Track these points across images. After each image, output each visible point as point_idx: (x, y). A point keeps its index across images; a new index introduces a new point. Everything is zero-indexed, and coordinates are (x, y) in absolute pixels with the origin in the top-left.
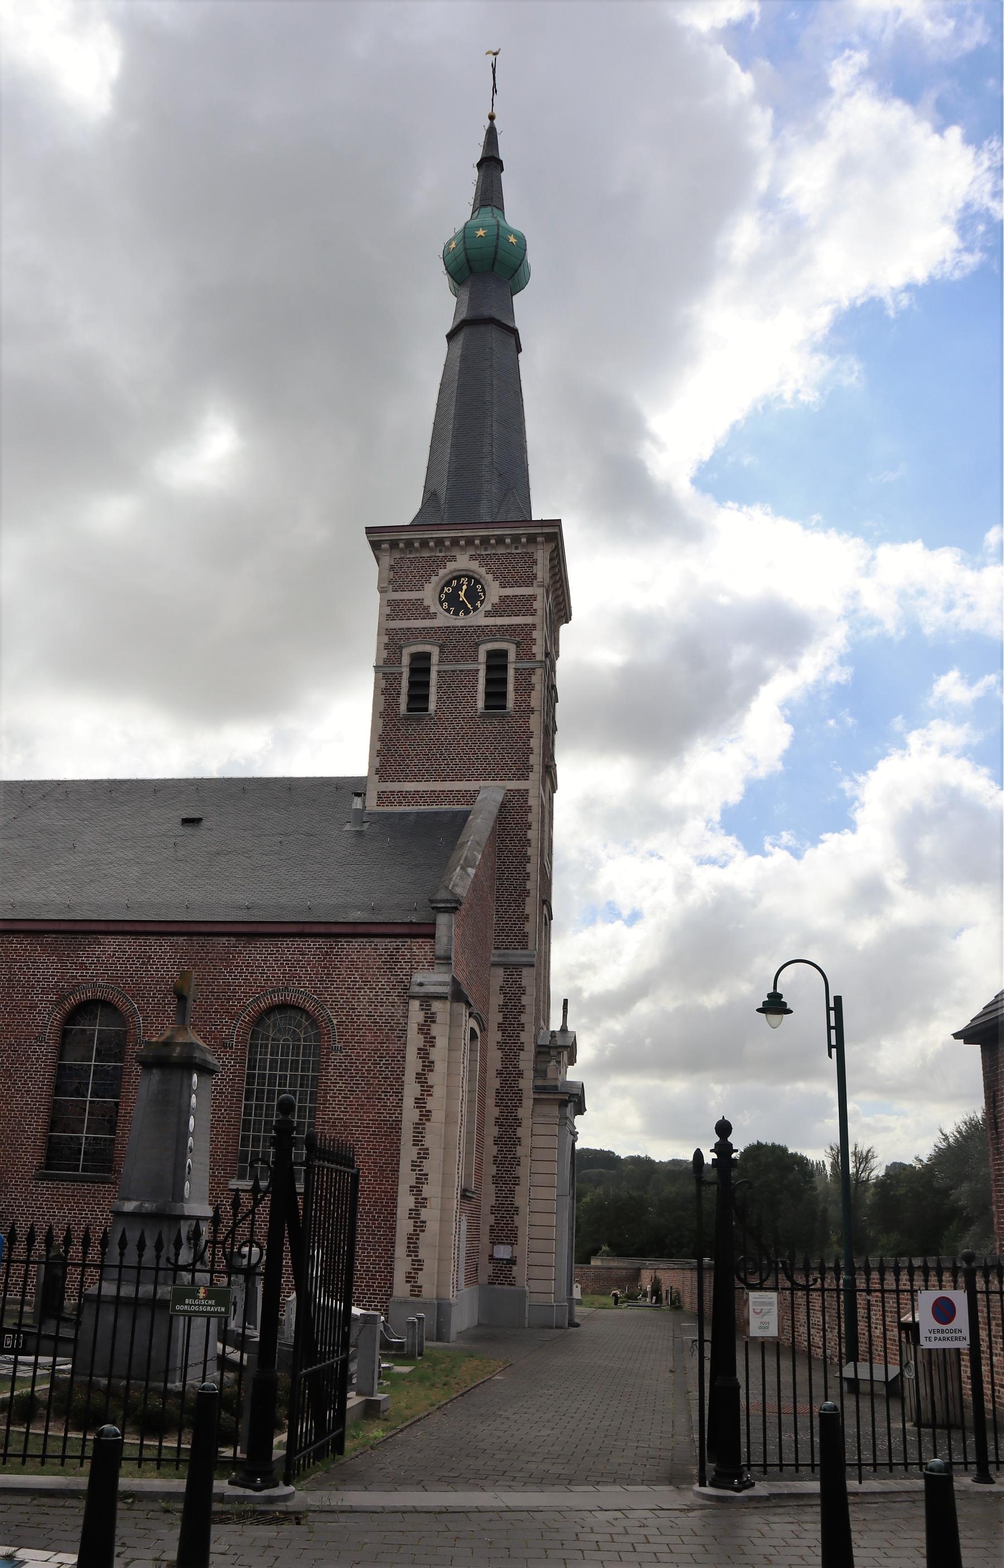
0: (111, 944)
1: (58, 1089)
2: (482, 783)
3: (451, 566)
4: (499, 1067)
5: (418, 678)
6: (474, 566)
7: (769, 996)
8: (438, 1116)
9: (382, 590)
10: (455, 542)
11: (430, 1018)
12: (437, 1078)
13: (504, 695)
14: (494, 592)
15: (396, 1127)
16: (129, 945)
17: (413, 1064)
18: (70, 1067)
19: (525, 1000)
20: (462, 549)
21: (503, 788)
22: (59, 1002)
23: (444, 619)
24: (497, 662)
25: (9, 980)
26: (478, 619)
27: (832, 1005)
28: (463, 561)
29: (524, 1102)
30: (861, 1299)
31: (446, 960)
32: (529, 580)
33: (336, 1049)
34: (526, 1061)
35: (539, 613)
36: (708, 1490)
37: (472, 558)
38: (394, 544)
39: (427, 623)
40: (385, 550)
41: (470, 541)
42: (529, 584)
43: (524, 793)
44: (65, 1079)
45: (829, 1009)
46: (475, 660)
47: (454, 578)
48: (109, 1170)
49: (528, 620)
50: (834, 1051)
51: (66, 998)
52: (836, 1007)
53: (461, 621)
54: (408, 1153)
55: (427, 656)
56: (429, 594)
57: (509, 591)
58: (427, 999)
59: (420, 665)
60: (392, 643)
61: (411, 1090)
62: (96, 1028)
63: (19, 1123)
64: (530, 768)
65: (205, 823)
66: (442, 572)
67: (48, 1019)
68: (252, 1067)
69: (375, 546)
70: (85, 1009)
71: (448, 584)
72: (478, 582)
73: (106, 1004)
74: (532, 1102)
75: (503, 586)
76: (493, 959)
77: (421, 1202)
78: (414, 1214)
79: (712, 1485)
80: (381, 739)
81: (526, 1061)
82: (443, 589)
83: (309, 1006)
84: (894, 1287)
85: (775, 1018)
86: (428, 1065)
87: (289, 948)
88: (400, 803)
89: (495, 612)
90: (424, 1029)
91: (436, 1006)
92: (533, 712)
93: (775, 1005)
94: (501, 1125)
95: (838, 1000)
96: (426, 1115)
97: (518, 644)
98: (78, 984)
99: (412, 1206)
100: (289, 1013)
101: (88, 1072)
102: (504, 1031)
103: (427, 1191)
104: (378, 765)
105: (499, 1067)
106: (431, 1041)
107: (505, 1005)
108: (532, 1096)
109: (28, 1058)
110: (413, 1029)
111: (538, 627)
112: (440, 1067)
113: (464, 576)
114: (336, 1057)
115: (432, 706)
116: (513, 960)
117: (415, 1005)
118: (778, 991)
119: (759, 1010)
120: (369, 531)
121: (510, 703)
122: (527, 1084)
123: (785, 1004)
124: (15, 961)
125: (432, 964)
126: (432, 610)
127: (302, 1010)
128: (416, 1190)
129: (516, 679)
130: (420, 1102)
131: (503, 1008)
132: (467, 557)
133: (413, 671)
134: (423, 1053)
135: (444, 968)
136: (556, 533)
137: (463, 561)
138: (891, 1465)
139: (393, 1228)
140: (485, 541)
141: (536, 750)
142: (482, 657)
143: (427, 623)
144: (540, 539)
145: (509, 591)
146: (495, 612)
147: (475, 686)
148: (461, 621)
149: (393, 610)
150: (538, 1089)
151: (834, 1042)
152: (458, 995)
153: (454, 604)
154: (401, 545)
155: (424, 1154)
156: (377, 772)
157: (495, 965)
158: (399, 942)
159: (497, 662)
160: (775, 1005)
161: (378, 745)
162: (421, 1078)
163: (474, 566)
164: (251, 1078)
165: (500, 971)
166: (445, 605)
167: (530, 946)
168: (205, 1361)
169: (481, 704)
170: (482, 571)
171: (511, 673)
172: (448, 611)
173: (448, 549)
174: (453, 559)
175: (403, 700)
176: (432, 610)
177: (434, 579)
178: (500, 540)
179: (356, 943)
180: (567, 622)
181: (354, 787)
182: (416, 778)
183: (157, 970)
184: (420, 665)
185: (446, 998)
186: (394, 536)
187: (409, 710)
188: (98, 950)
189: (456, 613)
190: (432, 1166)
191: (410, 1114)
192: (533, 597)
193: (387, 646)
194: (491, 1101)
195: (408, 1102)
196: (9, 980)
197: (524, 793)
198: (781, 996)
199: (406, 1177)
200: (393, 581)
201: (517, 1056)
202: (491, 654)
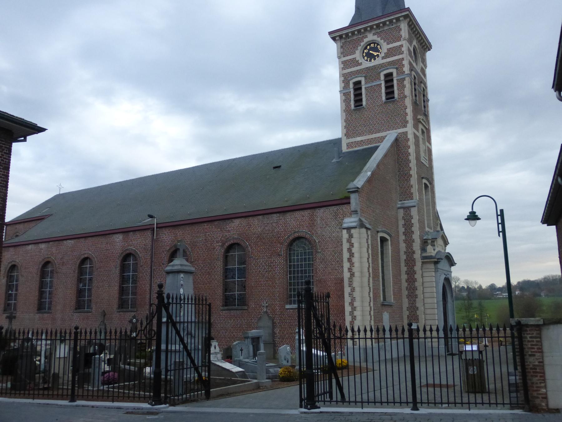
0: (237, 222)
1: (226, 277)
2: (388, 132)
3: (366, 40)
4: (405, 250)
5: (389, 84)
6: (375, 38)
7: (470, 213)
8: (357, 274)
9: (339, 58)
10: (365, 29)
11: (351, 236)
12: (355, 260)
13: (393, 92)
14: (385, 47)
15: (342, 280)
16: (244, 222)
17: (346, 255)
18: (229, 269)
19: (413, 221)
20: (370, 31)
21: (396, 133)
22: (222, 246)
23: (366, 64)
24: (389, 78)
25: (205, 240)
26: (378, 61)
27: (499, 213)
28: (371, 37)
29: (417, 263)
30: (415, 341)
31: (355, 212)
32: (399, 39)
33: (318, 253)
34: (417, 246)
35: (405, 52)
36: (303, 410)
37: (374, 34)
38: (341, 37)
39: (358, 68)
40: (338, 40)
41: (371, 27)
42: (399, 40)
43: (406, 133)
44: (227, 272)
45: (498, 215)
46: (380, 79)
47: (368, 45)
48: (245, 305)
49: (400, 57)
50: (501, 234)
51: (225, 244)
52: (501, 214)
53: (373, 63)
54: (347, 290)
55: (391, 74)
56: (358, 55)
57: (391, 46)
58: (349, 229)
59: (358, 85)
60: (345, 79)
61: (346, 265)
62: (236, 253)
63: (214, 291)
64: (407, 122)
65: (282, 167)
66: (362, 44)
67: (220, 251)
68: (290, 262)
69: (334, 39)
70: (231, 247)
71: (366, 48)
72: (378, 44)
73: (238, 244)
74: (421, 263)
75: (388, 44)
76: (399, 206)
77: (354, 309)
78: (351, 313)
79: (305, 408)
80: (345, 121)
81: (417, 246)
82: (363, 53)
83: (308, 236)
84: (423, 336)
85: (473, 222)
86: (352, 255)
87: (298, 214)
88: (356, 147)
89: (387, 56)
90: (349, 241)
91: (353, 231)
92: (406, 97)
93: (473, 217)
94: (408, 274)
95: (502, 211)
96: (352, 275)
97: (397, 69)
98: (228, 238)
99: (350, 310)
100: (301, 240)
101: (235, 270)
102: (405, 235)
103: (356, 304)
104: (345, 132)
105: (405, 250)
106: (352, 245)
107: (405, 224)
108: (421, 261)
109: (215, 267)
110: (345, 241)
111: (405, 59)
112: (356, 255)
113: (372, 43)
114: (319, 255)
115: (364, 103)
116: (406, 205)
117: (345, 232)
118: (474, 210)
119: (466, 219)
120: (330, 33)
121: (396, 96)
122: (417, 255)
123: (477, 216)
124: (206, 232)
125: (351, 214)
126: (360, 62)
127: (302, 238)
128: (351, 304)
129: (398, 84)
130: (350, 270)
131: (404, 225)
132: (372, 34)
133: (386, 82)
134: (350, 250)
135: (355, 216)
136: (408, 14)
137: (371, 37)
138: (455, 403)
139: (344, 320)
140: (378, 26)
141: (409, 114)
142: (382, 78)
143: (358, 68)
144: (401, 19)
145: (391, 46)
146: (387, 56)
147: (381, 91)
148: (373, 63)
149: (345, 65)
150: (424, 258)
151: (501, 230)
152: (362, 225)
153: (371, 57)
154: (344, 36)
155: (353, 290)
156: (345, 135)
157: (399, 208)
158: (338, 207)
159: (389, 78)
160: (473, 217)
161: (344, 124)
162: (350, 260)
163: (375, 38)
164: (290, 266)
165: (401, 211)
166: (366, 58)
167: (414, 198)
168: (367, 372)
169: (384, 98)
170: (379, 39)
171: (395, 82)
172: (367, 60)
173: (363, 33)
174: (366, 37)
175: (352, 103)
176: (360, 62)
177: (359, 48)
178: (384, 23)
179: (322, 210)
180: (429, 50)
181: (336, 143)
182: (360, 135)
183: (253, 230)
184: (357, 86)
185: (356, 227)
186: (340, 33)
187: (355, 106)
188: (232, 225)
189: (370, 61)
190: (357, 294)
191: (346, 275)
192: (402, 46)
193: (343, 82)
194: (403, 264)
195: (346, 270)
196: (205, 240)
197: (406, 133)
198: (475, 213)
199: (347, 299)
200: (343, 52)
201: (412, 245)
202: (386, 76)
